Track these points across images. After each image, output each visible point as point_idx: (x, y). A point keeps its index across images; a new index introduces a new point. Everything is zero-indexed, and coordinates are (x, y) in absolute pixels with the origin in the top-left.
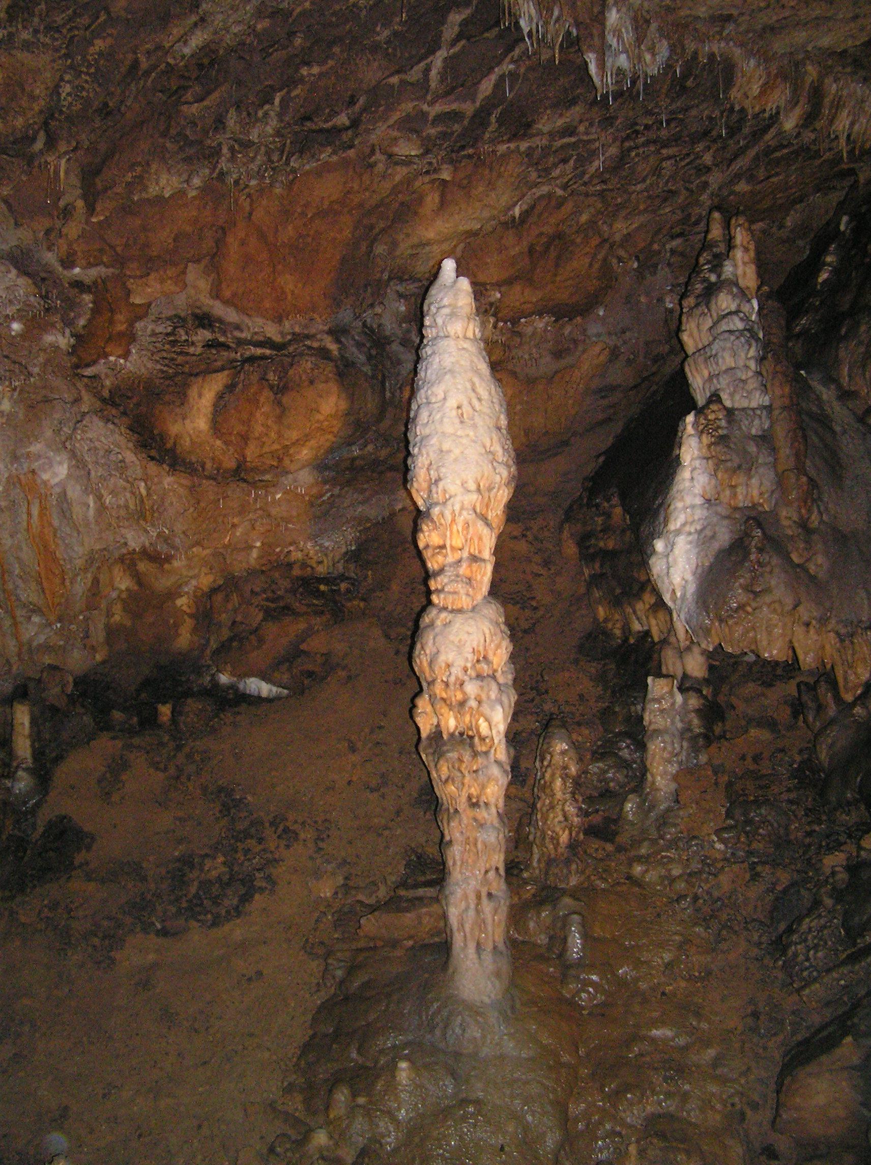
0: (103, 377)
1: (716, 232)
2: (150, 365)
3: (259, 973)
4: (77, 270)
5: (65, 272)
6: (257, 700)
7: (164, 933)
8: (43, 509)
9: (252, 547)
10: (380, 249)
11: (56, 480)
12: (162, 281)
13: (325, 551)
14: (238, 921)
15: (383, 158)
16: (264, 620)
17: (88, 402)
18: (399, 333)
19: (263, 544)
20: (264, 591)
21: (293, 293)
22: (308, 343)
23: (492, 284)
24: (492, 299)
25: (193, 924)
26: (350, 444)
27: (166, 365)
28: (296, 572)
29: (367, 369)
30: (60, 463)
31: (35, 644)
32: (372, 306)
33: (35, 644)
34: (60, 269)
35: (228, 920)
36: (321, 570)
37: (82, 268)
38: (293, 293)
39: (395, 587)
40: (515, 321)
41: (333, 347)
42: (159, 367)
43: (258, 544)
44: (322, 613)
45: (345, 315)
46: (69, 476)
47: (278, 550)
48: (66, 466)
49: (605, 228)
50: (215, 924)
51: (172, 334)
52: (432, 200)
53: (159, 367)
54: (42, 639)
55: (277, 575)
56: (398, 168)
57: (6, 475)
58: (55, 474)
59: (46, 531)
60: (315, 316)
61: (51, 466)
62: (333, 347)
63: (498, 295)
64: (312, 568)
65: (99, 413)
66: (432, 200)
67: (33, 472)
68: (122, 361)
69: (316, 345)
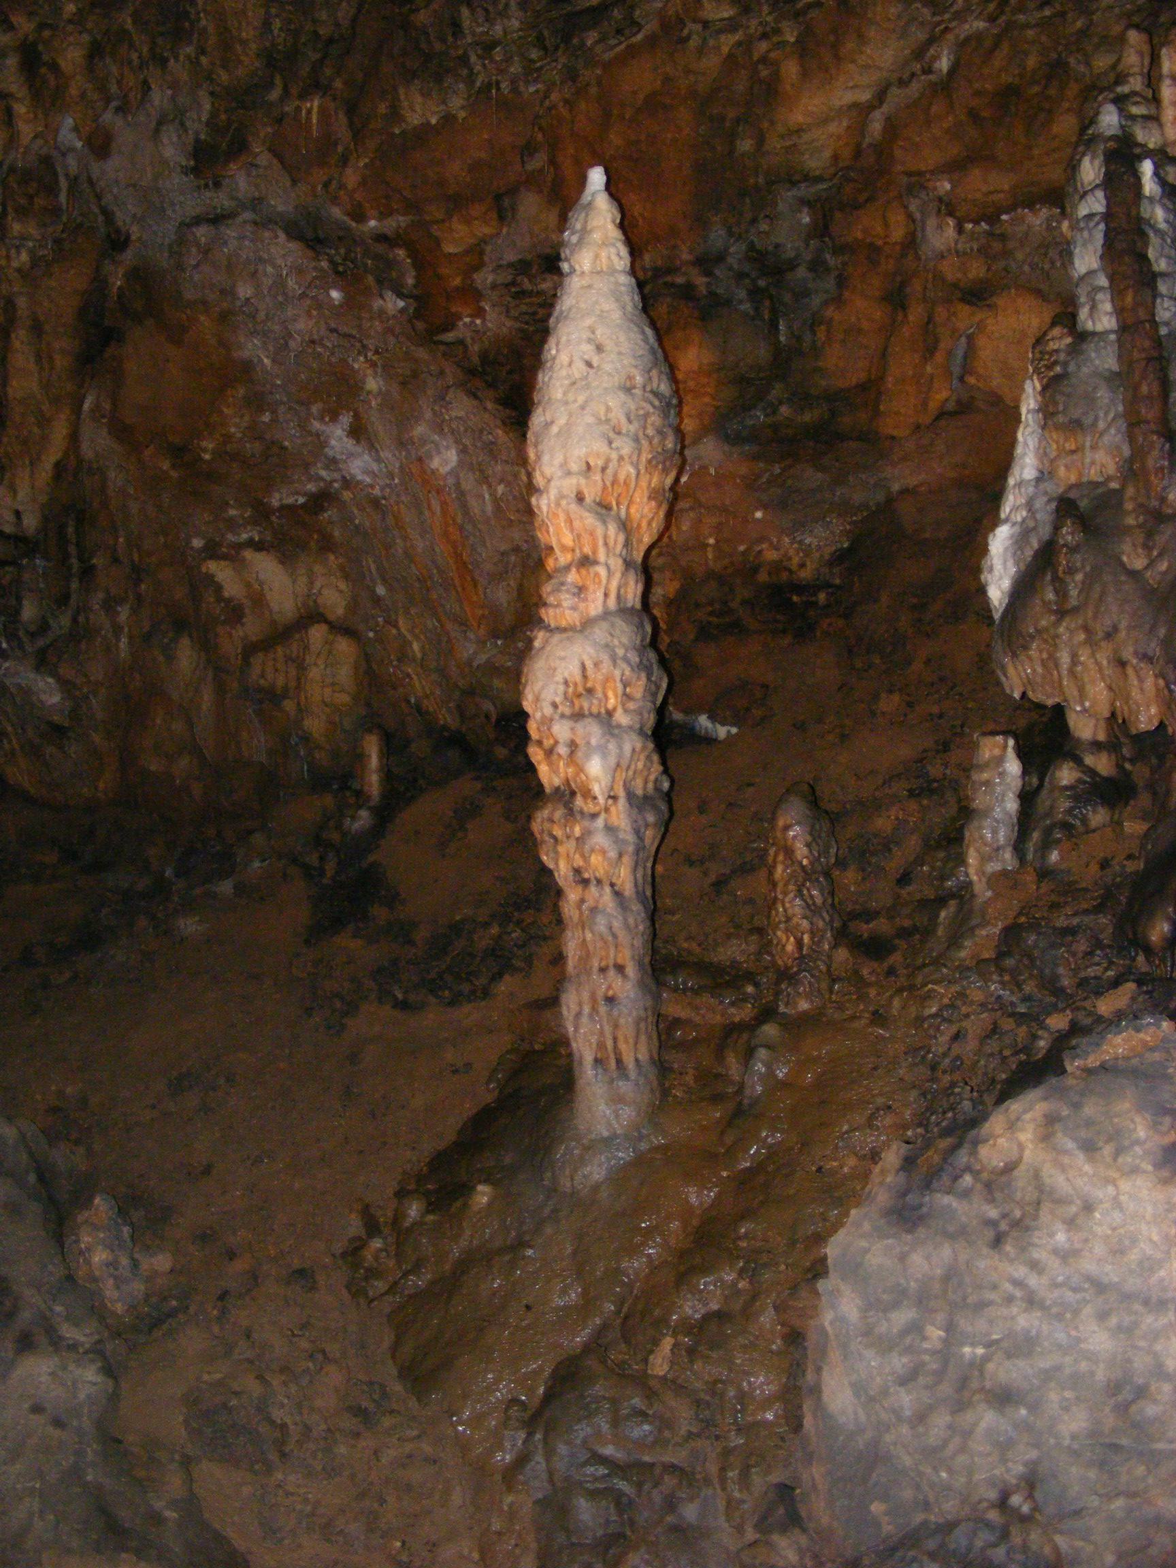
0: (469, 341)
1: (1133, 59)
2: (509, 323)
3: (468, 1065)
4: (373, 223)
5: (360, 226)
6: (710, 741)
7: (404, 1006)
8: (444, 504)
9: (705, 546)
10: (745, 145)
11: (447, 468)
12: (468, 222)
13: (807, 552)
14: (483, 1003)
15: (698, 27)
16: (696, 640)
17: (452, 373)
18: (808, 256)
19: (717, 541)
20: (711, 604)
21: (642, 215)
22: (669, 279)
23: (932, 172)
24: (941, 192)
25: (432, 999)
26: (747, 408)
27: (527, 323)
28: (763, 577)
29: (746, 307)
30: (447, 448)
31: (475, 664)
32: (754, 221)
33: (475, 664)
34: (354, 224)
35: (470, 1001)
36: (806, 574)
37: (379, 220)
38: (642, 215)
39: (884, 599)
40: (993, 219)
41: (700, 281)
42: (518, 325)
43: (711, 541)
44: (784, 632)
45: (717, 236)
46: (461, 463)
47: (742, 548)
48: (454, 452)
49: (1082, 68)
50: (452, 1003)
51: (513, 283)
52: (791, 69)
53: (518, 325)
54: (482, 658)
55: (738, 581)
56: (723, 38)
57: (397, 465)
58: (446, 462)
59: (451, 529)
60: (679, 242)
61: (439, 453)
62: (700, 281)
63: (948, 186)
64: (790, 571)
65: (461, 385)
66: (791, 69)
67: (420, 460)
68: (478, 322)
69: (680, 280)
